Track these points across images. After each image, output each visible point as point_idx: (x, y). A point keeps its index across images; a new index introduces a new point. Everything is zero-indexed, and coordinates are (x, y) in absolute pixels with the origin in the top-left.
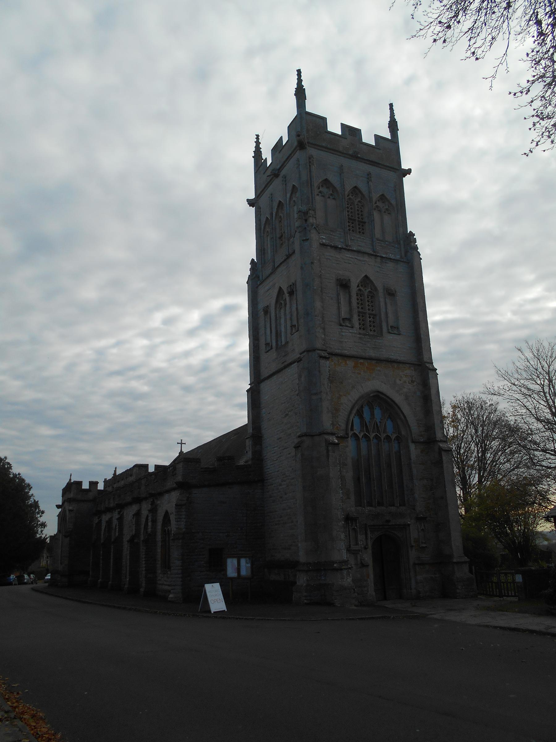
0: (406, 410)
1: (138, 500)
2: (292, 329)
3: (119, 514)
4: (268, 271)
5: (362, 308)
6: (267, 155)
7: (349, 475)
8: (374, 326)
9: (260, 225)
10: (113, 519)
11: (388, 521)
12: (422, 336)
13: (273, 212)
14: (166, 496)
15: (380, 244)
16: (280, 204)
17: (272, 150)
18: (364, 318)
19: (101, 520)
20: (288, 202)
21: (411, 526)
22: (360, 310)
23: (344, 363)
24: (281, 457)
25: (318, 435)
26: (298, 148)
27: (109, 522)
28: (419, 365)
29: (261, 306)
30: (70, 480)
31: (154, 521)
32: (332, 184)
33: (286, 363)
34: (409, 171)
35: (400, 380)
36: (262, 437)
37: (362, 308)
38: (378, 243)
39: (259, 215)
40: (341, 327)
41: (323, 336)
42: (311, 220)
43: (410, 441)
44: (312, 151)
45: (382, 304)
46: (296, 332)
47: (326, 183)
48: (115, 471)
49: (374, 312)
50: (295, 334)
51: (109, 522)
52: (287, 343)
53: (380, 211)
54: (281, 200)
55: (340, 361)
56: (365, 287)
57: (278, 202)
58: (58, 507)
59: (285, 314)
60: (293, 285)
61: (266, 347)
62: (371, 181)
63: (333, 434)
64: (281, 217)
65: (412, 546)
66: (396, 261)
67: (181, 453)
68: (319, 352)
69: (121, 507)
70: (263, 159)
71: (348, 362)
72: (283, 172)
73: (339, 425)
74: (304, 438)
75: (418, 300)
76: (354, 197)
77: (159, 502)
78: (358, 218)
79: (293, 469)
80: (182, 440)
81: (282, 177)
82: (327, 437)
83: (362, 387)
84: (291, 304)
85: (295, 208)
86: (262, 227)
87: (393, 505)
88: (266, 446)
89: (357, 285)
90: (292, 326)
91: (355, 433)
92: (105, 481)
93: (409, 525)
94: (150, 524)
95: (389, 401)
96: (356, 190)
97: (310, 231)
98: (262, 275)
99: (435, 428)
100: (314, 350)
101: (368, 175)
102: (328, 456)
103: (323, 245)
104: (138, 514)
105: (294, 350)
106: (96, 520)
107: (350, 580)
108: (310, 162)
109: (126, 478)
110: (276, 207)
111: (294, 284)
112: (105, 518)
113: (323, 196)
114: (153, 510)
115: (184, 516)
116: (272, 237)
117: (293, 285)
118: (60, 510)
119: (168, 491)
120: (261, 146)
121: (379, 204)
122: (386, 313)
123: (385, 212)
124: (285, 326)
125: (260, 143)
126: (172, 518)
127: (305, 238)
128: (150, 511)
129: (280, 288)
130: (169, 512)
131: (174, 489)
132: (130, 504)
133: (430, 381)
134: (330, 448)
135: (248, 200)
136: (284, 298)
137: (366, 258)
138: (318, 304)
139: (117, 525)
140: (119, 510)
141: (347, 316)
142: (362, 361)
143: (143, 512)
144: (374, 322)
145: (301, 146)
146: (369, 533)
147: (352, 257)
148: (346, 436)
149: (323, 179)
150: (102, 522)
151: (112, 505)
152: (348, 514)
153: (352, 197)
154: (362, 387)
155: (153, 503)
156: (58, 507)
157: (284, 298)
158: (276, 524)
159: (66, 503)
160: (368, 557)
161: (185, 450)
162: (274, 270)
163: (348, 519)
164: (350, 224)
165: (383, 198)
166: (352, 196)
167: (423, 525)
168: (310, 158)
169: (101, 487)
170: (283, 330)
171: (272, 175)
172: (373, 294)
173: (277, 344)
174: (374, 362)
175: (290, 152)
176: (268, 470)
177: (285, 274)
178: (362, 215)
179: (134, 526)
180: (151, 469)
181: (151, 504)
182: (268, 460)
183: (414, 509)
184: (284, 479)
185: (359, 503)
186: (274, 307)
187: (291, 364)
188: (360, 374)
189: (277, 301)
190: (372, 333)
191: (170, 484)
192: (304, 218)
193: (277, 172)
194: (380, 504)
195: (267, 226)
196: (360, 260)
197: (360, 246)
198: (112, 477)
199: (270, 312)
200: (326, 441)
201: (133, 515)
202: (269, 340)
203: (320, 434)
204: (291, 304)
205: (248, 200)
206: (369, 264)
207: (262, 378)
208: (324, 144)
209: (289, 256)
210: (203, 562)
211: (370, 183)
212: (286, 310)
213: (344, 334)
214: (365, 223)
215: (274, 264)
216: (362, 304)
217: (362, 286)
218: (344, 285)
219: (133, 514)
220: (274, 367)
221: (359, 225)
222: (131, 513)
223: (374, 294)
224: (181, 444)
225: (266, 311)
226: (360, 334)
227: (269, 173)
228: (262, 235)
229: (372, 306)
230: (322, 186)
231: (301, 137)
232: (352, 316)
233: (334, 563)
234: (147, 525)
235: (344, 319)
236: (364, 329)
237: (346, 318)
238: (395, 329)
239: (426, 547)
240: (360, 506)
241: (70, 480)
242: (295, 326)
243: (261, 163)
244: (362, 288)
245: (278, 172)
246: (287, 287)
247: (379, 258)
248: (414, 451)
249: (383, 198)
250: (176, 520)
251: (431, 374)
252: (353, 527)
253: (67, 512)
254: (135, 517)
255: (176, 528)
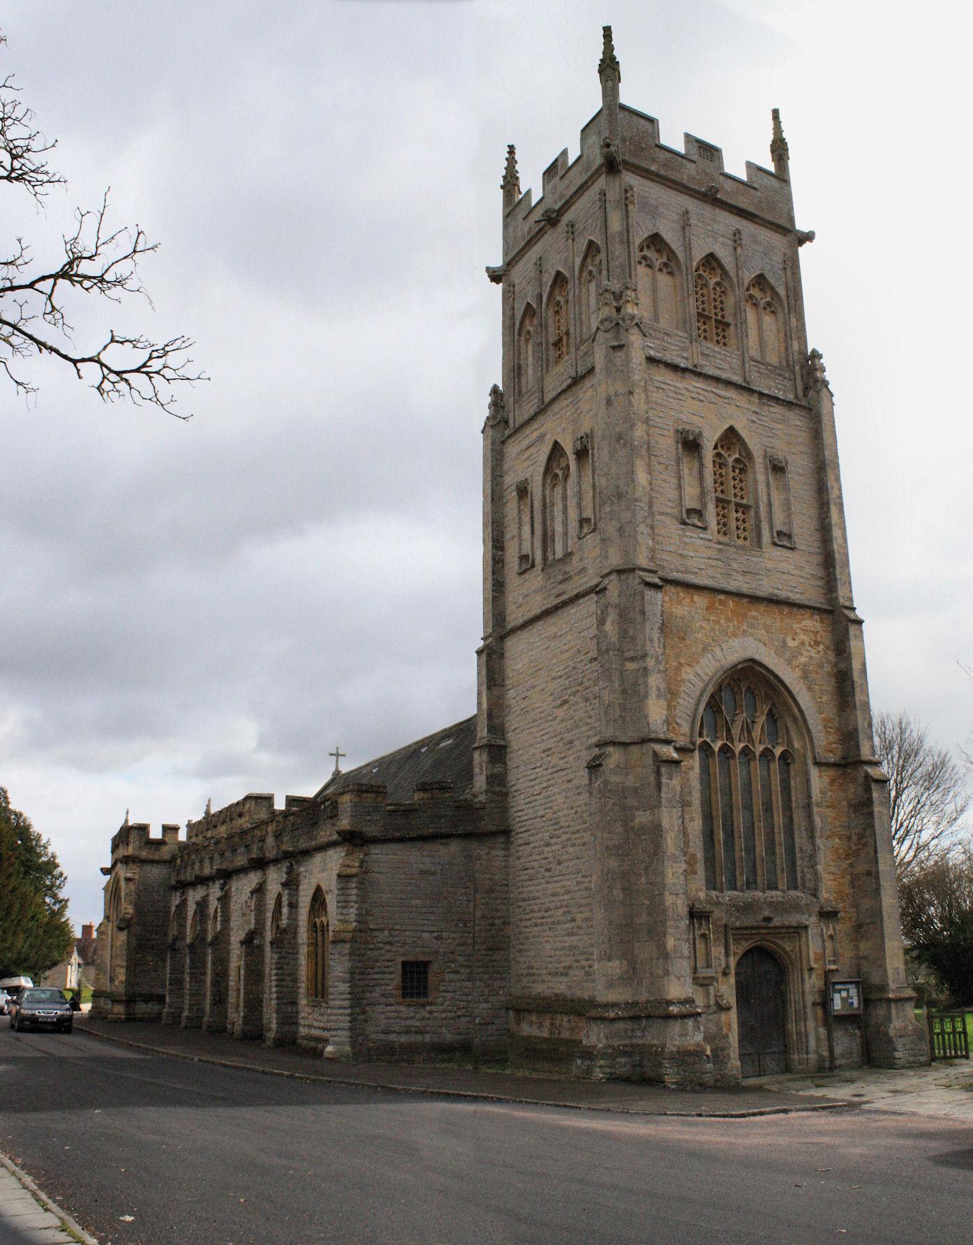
0: (804, 699)
1: (260, 864)
2: (581, 527)
3: (222, 889)
4: (529, 409)
5: (722, 492)
6: (532, 183)
7: (696, 825)
8: (745, 530)
9: (513, 318)
10: (211, 898)
11: (768, 919)
12: (837, 556)
13: (543, 294)
14: (318, 858)
15: (756, 369)
16: (560, 279)
17: (544, 174)
18: (725, 511)
19: (186, 900)
20: (577, 274)
21: (809, 929)
22: (719, 494)
23: (688, 600)
24: (551, 788)
25: (638, 743)
26: (604, 169)
27: (202, 905)
28: (830, 612)
29: (511, 480)
30: (126, 821)
31: (293, 906)
32: (667, 244)
33: (565, 597)
34: (809, 237)
35: (794, 640)
36: (505, 747)
37: (722, 492)
38: (754, 366)
39: (511, 299)
40: (683, 527)
41: (650, 543)
42: (630, 309)
43: (810, 761)
44: (629, 178)
45: (762, 487)
46: (590, 533)
47: (655, 241)
48: (208, 806)
49: (744, 501)
50: (588, 537)
51: (202, 905)
52: (568, 555)
53: (755, 305)
54: (561, 270)
55: (682, 595)
56: (729, 449)
57: (553, 273)
58: (105, 871)
59: (565, 498)
60: (587, 437)
61: (520, 565)
62: (740, 245)
63: (667, 742)
64: (558, 303)
65: (811, 969)
66: (789, 404)
67: (337, 773)
68: (642, 573)
69: (226, 876)
70: (520, 193)
71: (696, 598)
72: (566, 218)
73: (678, 724)
74: (610, 749)
75: (829, 483)
76: (707, 273)
77: (302, 869)
78: (716, 314)
79: (576, 813)
80: (337, 748)
81: (567, 225)
82: (657, 747)
83: (722, 650)
84: (580, 477)
85: (593, 286)
86: (517, 323)
87: (776, 888)
88: (515, 766)
89: (713, 443)
90: (583, 521)
91: (705, 741)
92: (190, 826)
93: (806, 927)
94: (285, 910)
95: (771, 678)
96: (711, 261)
97: (627, 330)
98: (515, 419)
99: (858, 737)
100: (632, 570)
101: (735, 234)
102: (659, 786)
103: (650, 360)
104: (259, 890)
105: (583, 570)
106: (176, 900)
107: (699, 1037)
108: (627, 198)
109: (231, 820)
110: (550, 284)
111: (589, 436)
112: (194, 896)
113: (649, 266)
114: (291, 884)
115: (354, 898)
116: (539, 341)
117: (587, 437)
118: (108, 877)
119: (323, 848)
120: (517, 167)
121: (755, 292)
122: (770, 504)
123: (765, 309)
124: (563, 521)
125: (516, 162)
126: (331, 901)
127: (616, 344)
128: (285, 885)
129: (556, 443)
130: (324, 888)
131: (332, 844)
132: (243, 870)
133: (852, 643)
134: (663, 770)
135: (488, 269)
136: (563, 465)
137: (731, 393)
138: (642, 477)
139: (219, 910)
140: (222, 881)
141: (697, 506)
142: (722, 597)
143: (269, 888)
144: (744, 521)
145: (611, 166)
146: (731, 941)
147: (706, 388)
148: (691, 746)
149: (651, 233)
150: (189, 902)
151: (207, 871)
152: (693, 904)
153: (703, 273)
154: (722, 650)
155: (290, 871)
156: (105, 871)
157: (563, 465)
158: (536, 925)
159: (119, 865)
160: (727, 990)
161: (345, 768)
162: (542, 410)
163: (696, 915)
164: (700, 324)
165: (760, 281)
166: (705, 272)
167: (831, 927)
168: (626, 191)
169: (182, 836)
170: (559, 528)
171: (545, 220)
172: (744, 465)
173: (545, 558)
174: (745, 600)
175: (585, 178)
176: (520, 814)
177: (568, 414)
178: (722, 310)
179: (253, 913)
180: (280, 805)
181: (288, 873)
182: (520, 795)
183: (815, 896)
184: (556, 833)
185: (712, 884)
186: (540, 483)
187: (578, 597)
188: (718, 622)
189: (548, 469)
190: (740, 542)
191: (326, 833)
192: (614, 304)
193: (554, 215)
194: (751, 884)
195: (527, 321)
196: (719, 396)
197: (719, 368)
198: (204, 818)
199: (532, 492)
200: (655, 754)
201: (250, 892)
202: (526, 549)
203: (644, 741)
204: (580, 477)
205: (488, 269)
206: (738, 404)
207: (509, 626)
208: (653, 168)
209: (576, 381)
210: (390, 988)
211: (739, 250)
212: (566, 488)
213: (688, 540)
214: (728, 325)
215: (543, 396)
216: (722, 484)
217: (722, 447)
218: (691, 444)
219: (251, 889)
220: (538, 604)
221: (717, 328)
222: (245, 887)
223: (745, 465)
224: (337, 755)
225: (523, 491)
226: (720, 543)
227: (537, 215)
228: (516, 337)
229: (742, 489)
230: (648, 247)
231: (613, 149)
232: (704, 505)
233: (670, 1003)
234: (280, 913)
235: (689, 511)
236: (725, 534)
237: (694, 509)
238: (784, 539)
239: (837, 970)
240: (715, 889)
241: (126, 821)
242: (588, 520)
243: (516, 201)
244: (723, 452)
245: (557, 216)
246: (575, 442)
247: (756, 395)
248: (818, 781)
249: (760, 281)
250: (340, 904)
251: (852, 629)
252: (702, 931)
253: (123, 883)
254: (255, 896)
255: (339, 920)
